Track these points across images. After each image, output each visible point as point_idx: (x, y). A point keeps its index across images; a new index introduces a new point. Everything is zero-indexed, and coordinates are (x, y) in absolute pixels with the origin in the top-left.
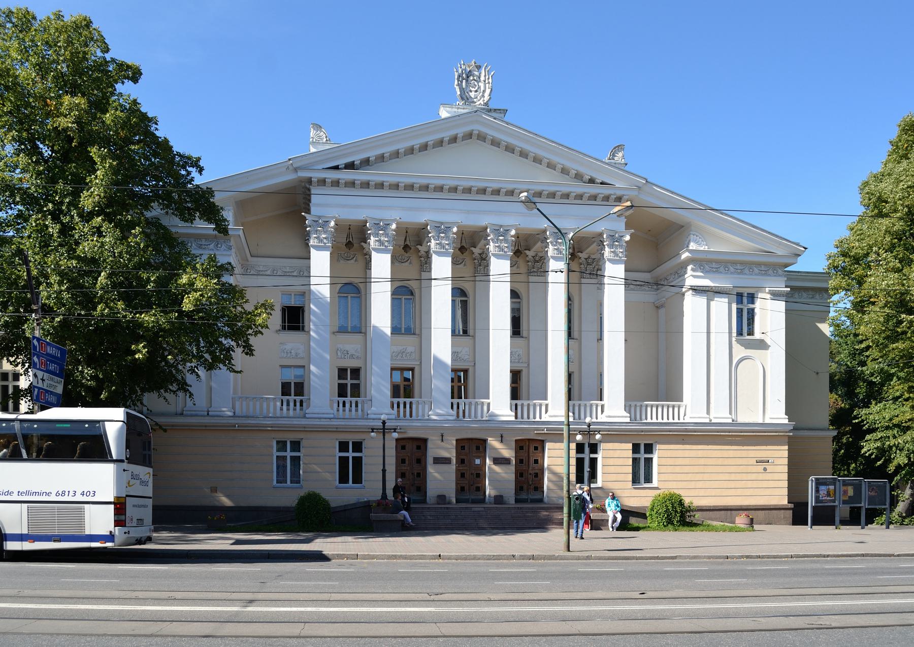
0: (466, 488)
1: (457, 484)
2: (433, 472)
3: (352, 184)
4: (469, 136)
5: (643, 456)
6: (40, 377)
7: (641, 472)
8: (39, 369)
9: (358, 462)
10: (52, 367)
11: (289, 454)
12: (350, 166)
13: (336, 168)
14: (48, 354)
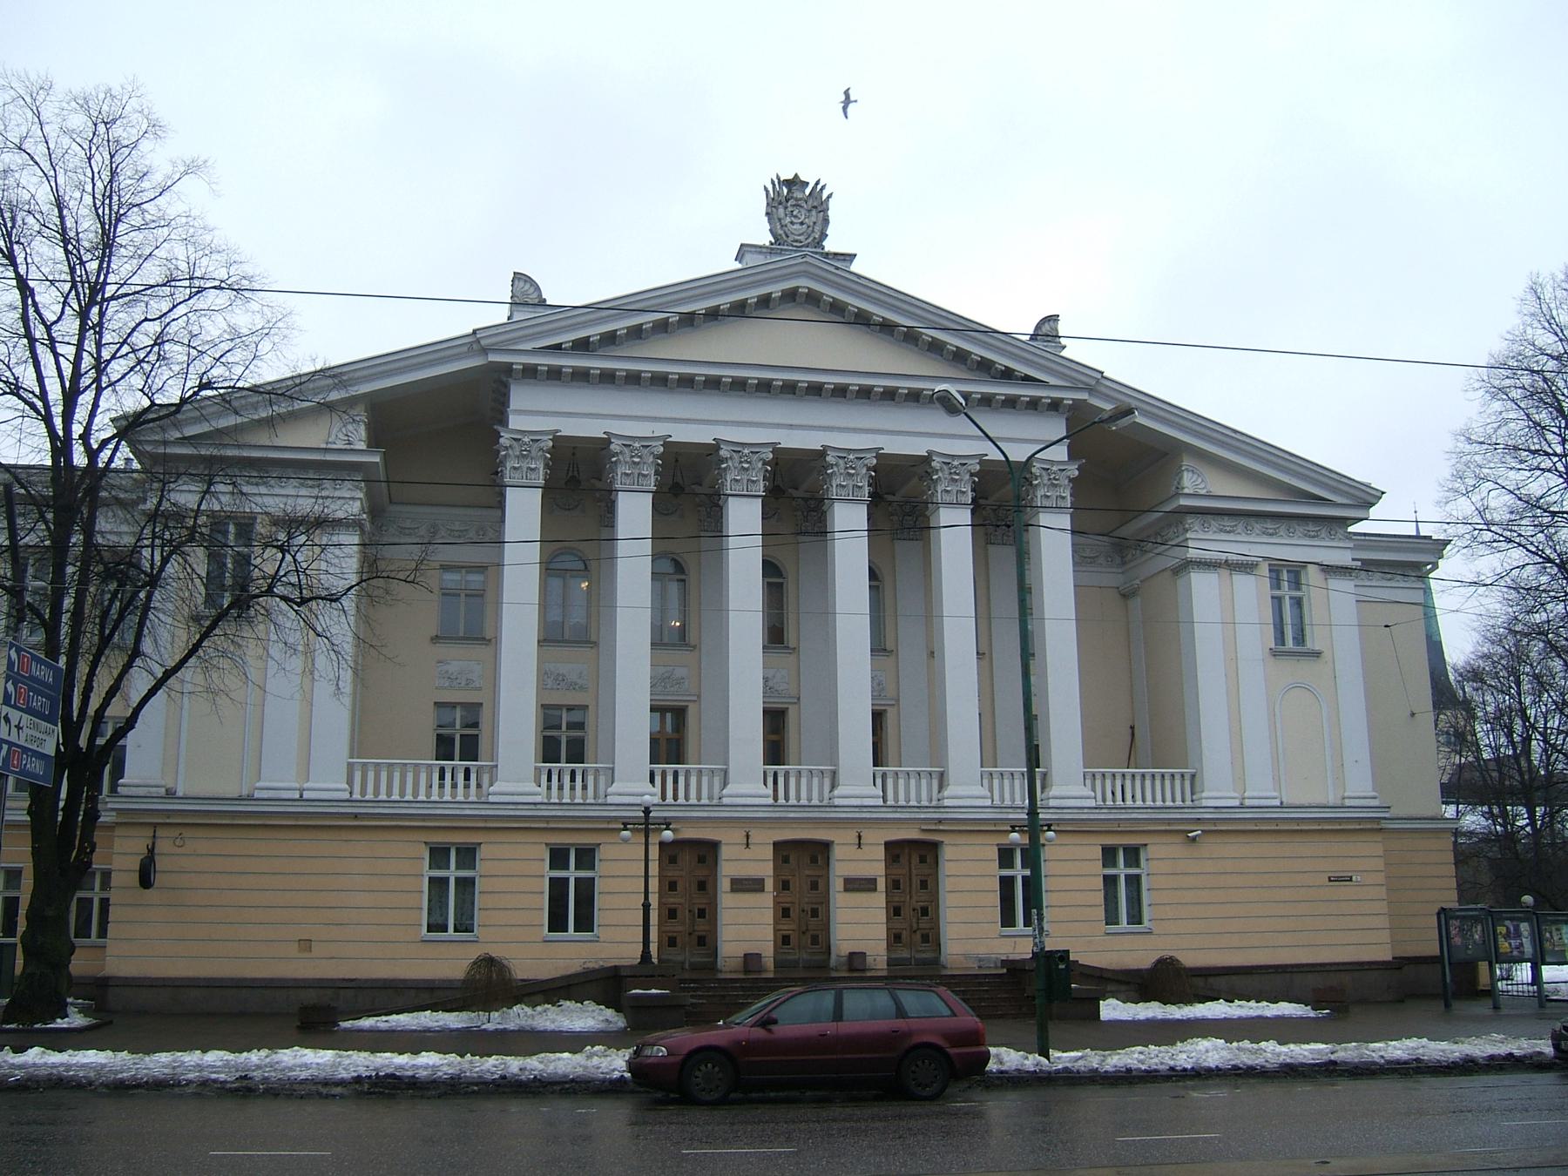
0: (905, 935)
1: (776, 931)
2: (730, 905)
3: (608, 378)
4: (791, 296)
5: (1121, 870)
6: (14, 722)
7: (1123, 898)
8: (15, 707)
9: (586, 891)
10: (38, 702)
11: (453, 873)
12: (582, 346)
13: (558, 347)
14: (32, 678)
